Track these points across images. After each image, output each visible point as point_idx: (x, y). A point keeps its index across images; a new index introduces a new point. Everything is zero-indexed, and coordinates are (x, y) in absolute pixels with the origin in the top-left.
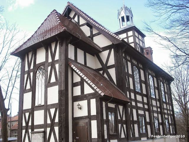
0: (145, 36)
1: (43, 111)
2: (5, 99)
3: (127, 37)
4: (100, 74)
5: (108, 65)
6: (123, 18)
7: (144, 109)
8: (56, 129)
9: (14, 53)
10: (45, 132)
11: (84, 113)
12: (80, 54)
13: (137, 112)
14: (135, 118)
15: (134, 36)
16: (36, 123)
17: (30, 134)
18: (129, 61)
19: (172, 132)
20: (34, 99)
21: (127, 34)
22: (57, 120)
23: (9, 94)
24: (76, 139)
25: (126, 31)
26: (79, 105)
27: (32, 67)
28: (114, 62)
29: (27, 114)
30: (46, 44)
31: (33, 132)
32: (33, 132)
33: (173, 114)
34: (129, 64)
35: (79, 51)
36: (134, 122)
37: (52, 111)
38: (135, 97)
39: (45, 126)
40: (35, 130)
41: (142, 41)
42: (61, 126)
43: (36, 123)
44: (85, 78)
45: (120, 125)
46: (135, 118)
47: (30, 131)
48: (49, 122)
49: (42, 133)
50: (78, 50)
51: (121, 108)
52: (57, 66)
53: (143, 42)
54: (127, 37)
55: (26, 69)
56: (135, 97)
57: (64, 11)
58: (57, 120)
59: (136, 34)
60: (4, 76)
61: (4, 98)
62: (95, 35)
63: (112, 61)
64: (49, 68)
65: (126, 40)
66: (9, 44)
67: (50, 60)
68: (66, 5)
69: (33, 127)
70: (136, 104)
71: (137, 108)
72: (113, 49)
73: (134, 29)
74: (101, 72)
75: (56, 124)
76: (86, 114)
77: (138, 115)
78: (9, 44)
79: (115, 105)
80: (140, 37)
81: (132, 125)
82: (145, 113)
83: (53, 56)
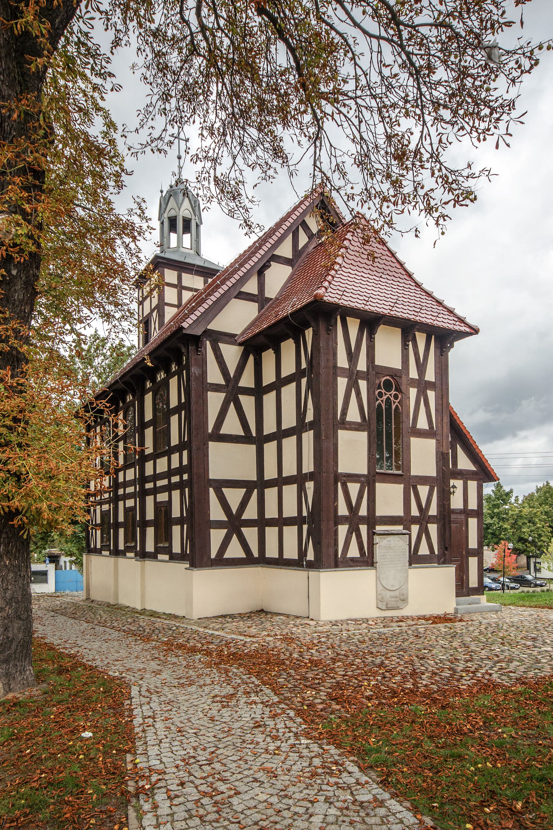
3: (180, 287)
29: (354, 488)
39: (405, 521)
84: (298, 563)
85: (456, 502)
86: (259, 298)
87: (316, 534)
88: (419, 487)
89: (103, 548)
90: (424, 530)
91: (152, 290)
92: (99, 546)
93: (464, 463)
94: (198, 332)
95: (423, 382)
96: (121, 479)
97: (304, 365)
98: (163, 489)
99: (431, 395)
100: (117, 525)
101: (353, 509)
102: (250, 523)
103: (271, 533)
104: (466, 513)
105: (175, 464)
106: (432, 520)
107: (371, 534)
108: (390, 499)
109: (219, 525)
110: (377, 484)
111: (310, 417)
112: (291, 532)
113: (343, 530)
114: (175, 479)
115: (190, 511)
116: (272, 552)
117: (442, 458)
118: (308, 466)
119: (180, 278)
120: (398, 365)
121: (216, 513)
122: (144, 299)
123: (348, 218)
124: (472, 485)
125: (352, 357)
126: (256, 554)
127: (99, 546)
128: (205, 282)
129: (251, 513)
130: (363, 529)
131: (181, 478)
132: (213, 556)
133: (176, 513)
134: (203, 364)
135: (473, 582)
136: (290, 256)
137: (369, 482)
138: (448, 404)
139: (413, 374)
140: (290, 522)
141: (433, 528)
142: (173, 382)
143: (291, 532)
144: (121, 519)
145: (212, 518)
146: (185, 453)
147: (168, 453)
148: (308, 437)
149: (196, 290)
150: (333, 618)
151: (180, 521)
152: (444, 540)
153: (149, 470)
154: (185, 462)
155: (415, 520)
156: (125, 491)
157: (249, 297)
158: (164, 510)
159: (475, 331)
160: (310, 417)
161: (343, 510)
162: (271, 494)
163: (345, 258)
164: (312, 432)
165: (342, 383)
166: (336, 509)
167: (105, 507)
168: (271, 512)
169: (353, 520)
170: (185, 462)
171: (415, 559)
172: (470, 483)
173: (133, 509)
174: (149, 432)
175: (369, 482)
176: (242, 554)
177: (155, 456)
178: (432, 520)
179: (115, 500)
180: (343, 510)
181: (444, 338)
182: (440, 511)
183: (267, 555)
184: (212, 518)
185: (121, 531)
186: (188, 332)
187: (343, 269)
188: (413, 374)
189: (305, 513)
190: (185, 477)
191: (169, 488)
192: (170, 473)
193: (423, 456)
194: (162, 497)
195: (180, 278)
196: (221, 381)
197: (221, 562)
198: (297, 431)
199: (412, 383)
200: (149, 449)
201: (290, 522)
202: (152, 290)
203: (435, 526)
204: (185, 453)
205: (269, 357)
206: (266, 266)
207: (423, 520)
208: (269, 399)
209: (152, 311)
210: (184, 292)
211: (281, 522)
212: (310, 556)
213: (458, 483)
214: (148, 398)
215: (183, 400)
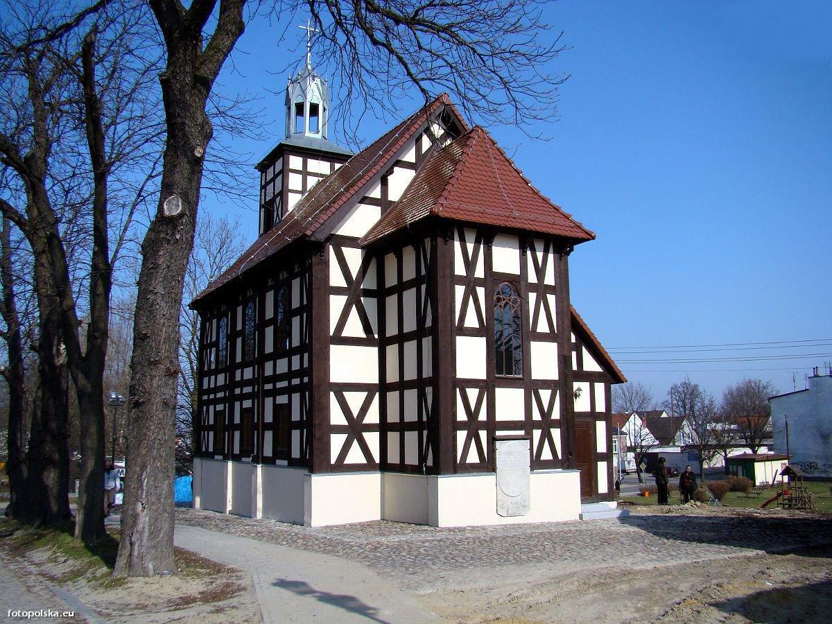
3: (305, 173)
29: (472, 394)
39: (527, 425)
83: (540, 272)
84: (416, 470)
85: (581, 405)
86: (383, 202)
87: (434, 440)
88: (541, 391)
89: (216, 452)
90: (546, 435)
91: (276, 176)
92: (211, 449)
93: (590, 364)
94: (321, 237)
95: (543, 287)
96: (238, 378)
97: (423, 272)
98: (282, 391)
99: (551, 299)
100: (232, 427)
101: (472, 415)
102: (370, 428)
103: (393, 437)
104: (593, 415)
105: (296, 366)
106: (555, 424)
107: (492, 440)
108: (510, 403)
109: (339, 429)
110: (496, 389)
111: (429, 323)
112: (411, 437)
113: (462, 436)
114: (296, 381)
115: (310, 414)
116: (393, 458)
117: (564, 361)
118: (427, 372)
119: (305, 164)
120: (516, 270)
121: (337, 417)
122: (267, 184)
123: (470, 127)
124: (600, 387)
125: (470, 265)
126: (377, 460)
127: (211, 449)
128: (332, 168)
129: (373, 417)
130: (483, 434)
131: (302, 381)
132: (333, 460)
133: (296, 416)
134: (326, 264)
135: (603, 487)
136: (413, 160)
137: (486, 388)
138: (569, 305)
139: (532, 278)
140: (411, 426)
141: (556, 433)
142: (296, 284)
143: (411, 437)
144: (237, 420)
145: (332, 423)
146: (306, 356)
147: (289, 354)
148: (427, 342)
149: (321, 175)
150: (451, 525)
151: (299, 425)
152: (568, 445)
153: (269, 369)
154: (306, 365)
155: (536, 425)
156: (242, 390)
157: (374, 202)
158: (282, 412)
159: (593, 238)
160: (429, 323)
161: (461, 416)
162: (393, 397)
163: (466, 163)
164: (431, 337)
165: (460, 291)
166: (454, 414)
167: (220, 407)
168: (393, 417)
169: (472, 426)
170: (306, 365)
171: (537, 463)
172: (597, 385)
173: (251, 410)
174: (269, 331)
175: (486, 388)
176: (363, 460)
177: (274, 357)
178: (555, 424)
179: (231, 400)
180: (461, 416)
181: (562, 245)
182: (563, 415)
183: (389, 461)
184: (332, 423)
185: (237, 434)
186: (313, 239)
187: (446, 209)
188: (532, 278)
189: (425, 419)
190: (306, 380)
191: (289, 391)
192: (290, 375)
193: (544, 360)
194: (283, 399)
195: (305, 164)
196: (343, 284)
197: (341, 467)
198: (418, 335)
199: (533, 288)
200: (269, 348)
201: (411, 426)
202: (276, 176)
203: (558, 430)
204: (306, 356)
205: (391, 262)
206: (390, 172)
207: (546, 424)
208: (392, 302)
209: (275, 197)
210: (309, 178)
211: (402, 427)
212: (430, 462)
213: (585, 386)
214: (270, 296)
215: (305, 303)
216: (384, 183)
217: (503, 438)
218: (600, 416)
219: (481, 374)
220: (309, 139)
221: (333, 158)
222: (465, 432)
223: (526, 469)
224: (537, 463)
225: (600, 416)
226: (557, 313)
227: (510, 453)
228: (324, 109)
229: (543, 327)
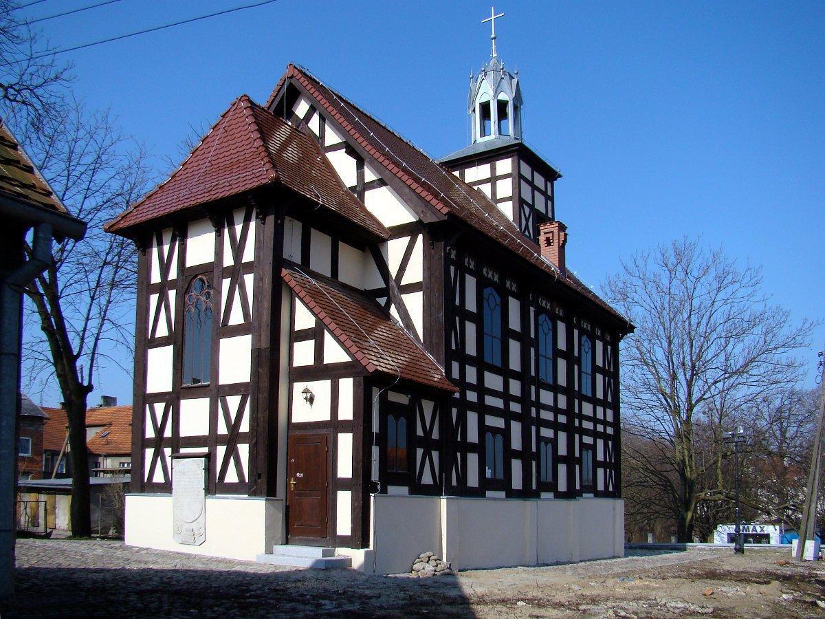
0: (560, 176)
1: (207, 400)
2: (79, 355)
3: (493, 180)
4: (378, 305)
5: (403, 283)
6: (485, 108)
7: (506, 414)
8: (244, 450)
9: (115, 227)
10: (210, 458)
11: (320, 412)
12: (321, 246)
13: (538, 432)
14: (473, 436)
15: (518, 178)
16: (184, 432)
17: (168, 460)
18: (472, 273)
19: (601, 487)
20: (179, 365)
21: (493, 169)
22: (245, 427)
23: (90, 342)
24: (296, 479)
25: (489, 156)
26: (306, 391)
27: (173, 274)
28: (218, 450)
29: (160, 408)
30: (218, 214)
31: (176, 456)
32: (176, 456)
33: (616, 438)
34: (471, 282)
35: (316, 235)
36: (467, 448)
37: (233, 402)
38: (480, 378)
39: (212, 440)
40: (183, 451)
41: (544, 193)
42: (256, 443)
43: (184, 432)
44: (327, 321)
45: (420, 452)
46: (473, 436)
47: (168, 451)
48: (222, 429)
49: (203, 459)
50: (316, 235)
51: (428, 407)
52: (249, 279)
53: (549, 198)
54: (493, 180)
55: (156, 278)
56: (480, 378)
57: (276, 97)
58: (245, 427)
59: (526, 170)
60: (71, 282)
61: (75, 353)
62: (371, 186)
63: (415, 273)
64: (226, 283)
65: (486, 189)
66: (85, 178)
67: (228, 261)
68: (285, 72)
69: (177, 442)
70: (481, 398)
71: (482, 410)
72: (420, 237)
73: (520, 152)
74: (382, 301)
75: (243, 438)
76: (326, 417)
77: (483, 429)
78: (85, 178)
79: (409, 396)
80: (539, 181)
81: (459, 454)
82: (595, 441)
83: (238, 250)
108: (195, 416)
137: (172, 401)
171: (214, 485)
216: (381, 183)
217: (198, 455)
218: (345, 426)
219: (168, 388)
220: (485, 144)
221: (461, 165)
222: (224, 448)
223: (199, 492)
224: (214, 485)
225: (345, 426)
226: (255, 296)
227: (184, 473)
228: (474, 111)
229: (236, 318)
